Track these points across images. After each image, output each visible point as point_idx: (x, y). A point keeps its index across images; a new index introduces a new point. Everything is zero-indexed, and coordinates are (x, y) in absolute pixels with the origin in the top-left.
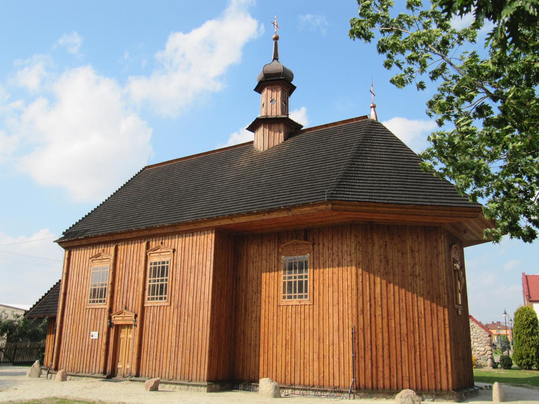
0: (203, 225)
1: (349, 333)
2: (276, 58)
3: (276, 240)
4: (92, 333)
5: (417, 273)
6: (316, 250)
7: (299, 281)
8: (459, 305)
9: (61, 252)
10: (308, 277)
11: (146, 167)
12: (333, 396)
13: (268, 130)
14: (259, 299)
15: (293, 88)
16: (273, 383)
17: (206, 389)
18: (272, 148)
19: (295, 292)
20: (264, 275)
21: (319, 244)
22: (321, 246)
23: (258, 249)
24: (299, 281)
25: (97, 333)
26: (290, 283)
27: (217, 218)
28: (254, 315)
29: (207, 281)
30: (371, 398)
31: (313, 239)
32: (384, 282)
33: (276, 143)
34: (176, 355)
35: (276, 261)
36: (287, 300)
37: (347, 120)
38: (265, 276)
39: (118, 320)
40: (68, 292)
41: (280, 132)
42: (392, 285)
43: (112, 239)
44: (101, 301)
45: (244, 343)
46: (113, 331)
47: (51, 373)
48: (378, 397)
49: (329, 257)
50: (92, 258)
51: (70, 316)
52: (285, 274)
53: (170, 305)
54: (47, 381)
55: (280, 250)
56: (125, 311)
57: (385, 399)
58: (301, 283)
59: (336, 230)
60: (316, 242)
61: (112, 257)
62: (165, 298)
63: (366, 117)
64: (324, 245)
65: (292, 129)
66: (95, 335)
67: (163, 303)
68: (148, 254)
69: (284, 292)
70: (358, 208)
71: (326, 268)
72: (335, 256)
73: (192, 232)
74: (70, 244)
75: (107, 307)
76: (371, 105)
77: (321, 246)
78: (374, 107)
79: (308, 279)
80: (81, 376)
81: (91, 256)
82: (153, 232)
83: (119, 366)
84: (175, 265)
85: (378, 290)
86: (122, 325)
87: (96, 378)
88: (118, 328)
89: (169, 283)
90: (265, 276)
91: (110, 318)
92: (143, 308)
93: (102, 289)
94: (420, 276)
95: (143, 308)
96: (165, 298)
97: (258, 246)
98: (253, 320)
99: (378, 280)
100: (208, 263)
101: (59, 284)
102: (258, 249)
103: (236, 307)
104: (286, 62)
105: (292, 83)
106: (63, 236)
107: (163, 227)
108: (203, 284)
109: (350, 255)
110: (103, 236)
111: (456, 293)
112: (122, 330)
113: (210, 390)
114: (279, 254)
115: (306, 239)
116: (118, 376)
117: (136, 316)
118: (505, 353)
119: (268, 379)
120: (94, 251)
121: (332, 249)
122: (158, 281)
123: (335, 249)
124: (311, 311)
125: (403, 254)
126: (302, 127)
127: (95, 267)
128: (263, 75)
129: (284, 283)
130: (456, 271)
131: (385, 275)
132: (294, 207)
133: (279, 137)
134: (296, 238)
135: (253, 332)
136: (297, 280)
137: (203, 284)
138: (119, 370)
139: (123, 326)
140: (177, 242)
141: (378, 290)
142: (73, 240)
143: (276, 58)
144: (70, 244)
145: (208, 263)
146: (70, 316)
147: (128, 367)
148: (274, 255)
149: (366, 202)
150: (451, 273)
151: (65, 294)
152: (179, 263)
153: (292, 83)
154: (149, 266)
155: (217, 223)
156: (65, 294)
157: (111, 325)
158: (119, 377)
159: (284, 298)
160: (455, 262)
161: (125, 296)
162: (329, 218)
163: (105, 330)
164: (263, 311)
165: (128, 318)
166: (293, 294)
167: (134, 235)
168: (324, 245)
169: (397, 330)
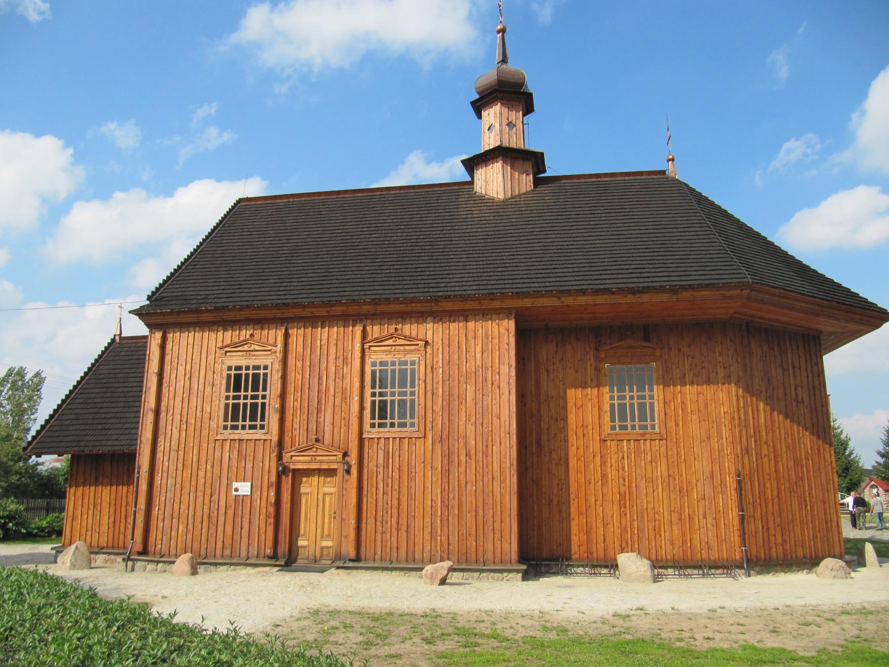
0: (496, 304)
1: (731, 482)
4: (235, 485)
7: (251, 404)
10: (268, 397)
12: (708, 574)
13: (509, 168)
14: (565, 428)
17: (520, 575)
18: (519, 195)
19: (244, 420)
20: (568, 391)
23: (556, 352)
24: (380, 401)
25: (249, 484)
26: (236, 407)
28: (554, 455)
29: (505, 397)
30: (769, 573)
32: (768, 408)
33: (523, 190)
34: (445, 521)
36: (377, 429)
37: (621, 173)
38: (573, 395)
40: (163, 408)
41: (527, 175)
42: (776, 413)
43: (279, 315)
45: (538, 499)
46: (287, 483)
47: (133, 560)
48: (776, 572)
50: (226, 347)
51: (173, 455)
52: (612, 391)
53: (425, 437)
54: (128, 574)
57: (783, 574)
58: (254, 406)
59: (701, 329)
61: (280, 346)
63: (664, 172)
68: (367, 346)
69: (373, 417)
70: (776, 299)
71: (685, 385)
73: (465, 315)
75: (275, 438)
76: (671, 157)
80: (216, 564)
81: (220, 345)
82: (382, 308)
83: (301, 543)
85: (762, 420)
86: (304, 470)
87: (255, 565)
88: (298, 475)
89: (419, 400)
90: (573, 395)
91: (280, 457)
97: (557, 346)
98: (554, 462)
99: (761, 404)
100: (505, 369)
102: (556, 352)
106: (148, 302)
110: (262, 307)
112: (304, 479)
113: (526, 576)
114: (599, 360)
115: (647, 339)
116: (299, 561)
119: (634, 554)
120: (229, 336)
128: (496, 82)
131: (769, 400)
132: (684, 288)
135: (555, 482)
136: (249, 401)
138: (301, 551)
139: (309, 473)
140: (430, 330)
141: (762, 420)
143: (504, 60)
145: (505, 369)
146: (173, 455)
148: (590, 361)
151: (157, 412)
154: (368, 369)
157: (283, 471)
158: (300, 562)
159: (373, 426)
163: (273, 479)
164: (572, 450)
167: (337, 310)
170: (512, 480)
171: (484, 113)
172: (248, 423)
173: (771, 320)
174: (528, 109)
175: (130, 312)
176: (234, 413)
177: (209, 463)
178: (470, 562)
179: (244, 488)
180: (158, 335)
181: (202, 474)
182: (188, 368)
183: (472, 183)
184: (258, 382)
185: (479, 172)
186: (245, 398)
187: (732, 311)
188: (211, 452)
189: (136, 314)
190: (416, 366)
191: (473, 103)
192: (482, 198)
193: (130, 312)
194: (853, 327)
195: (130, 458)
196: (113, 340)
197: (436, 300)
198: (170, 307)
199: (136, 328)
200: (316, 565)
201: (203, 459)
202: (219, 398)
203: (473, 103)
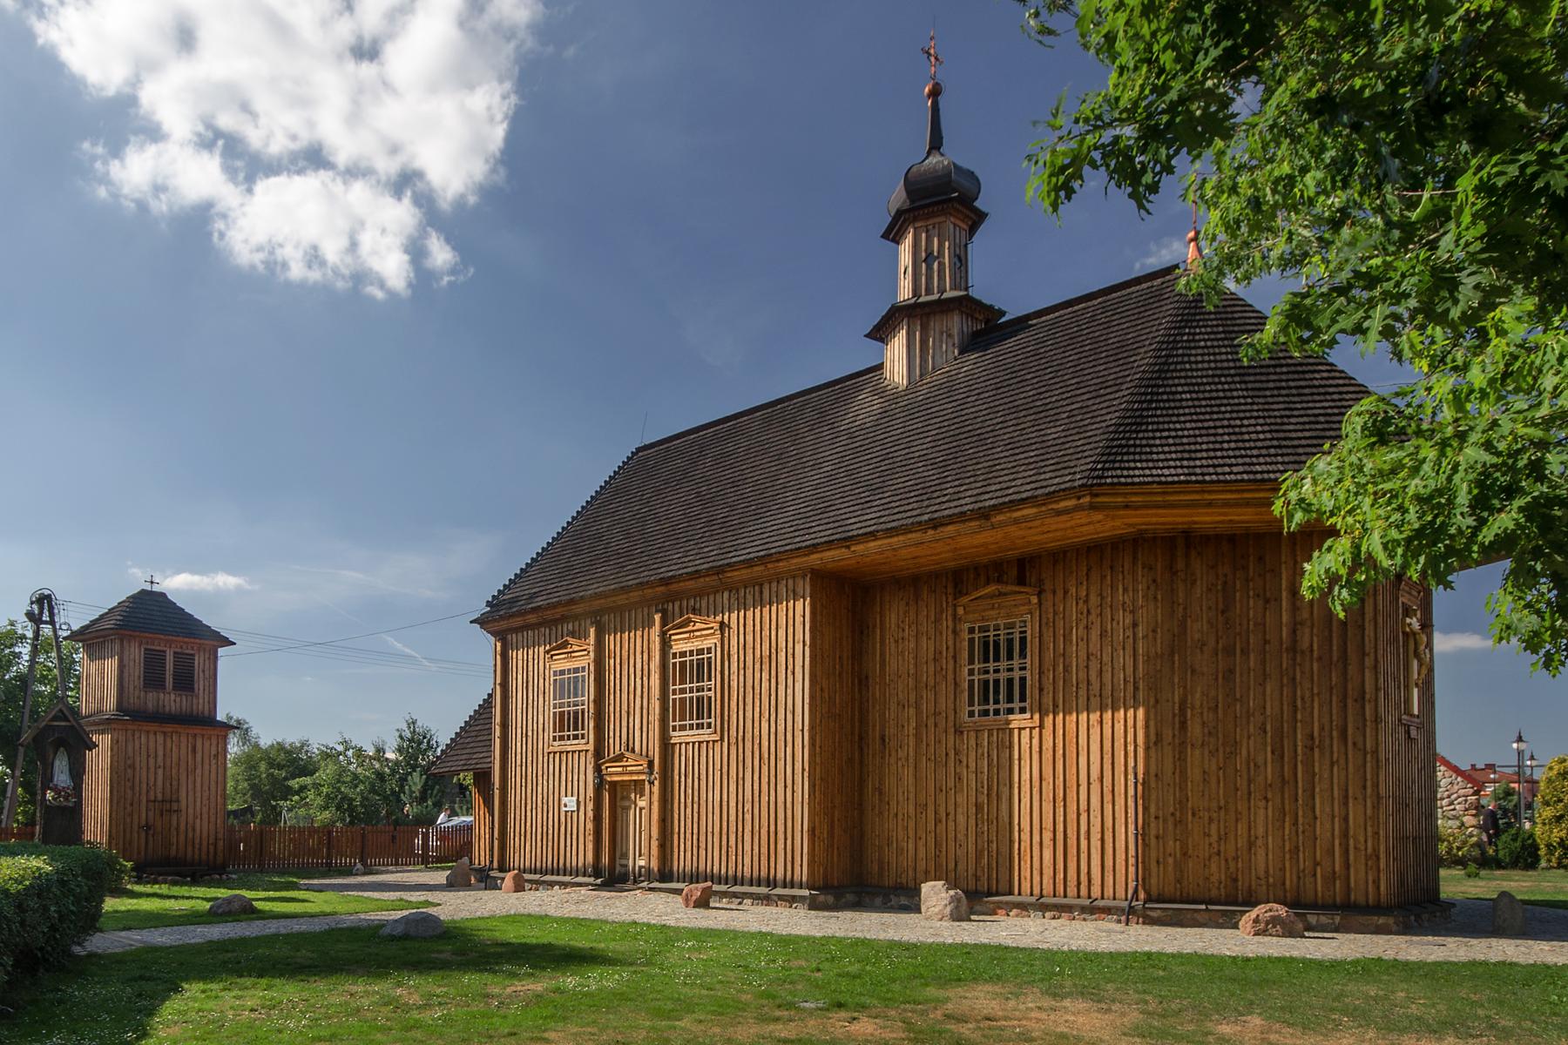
2: (936, 144)
3: (950, 590)
5: (1305, 645)
6: (1048, 605)
8: (1412, 715)
9: (485, 645)
11: (639, 450)
15: (981, 216)
16: (952, 892)
21: (1054, 592)
22: (1060, 594)
27: (814, 548)
31: (1041, 581)
35: (951, 637)
39: (614, 773)
44: (576, 737)
49: (1078, 621)
53: (722, 739)
55: (960, 611)
56: (627, 754)
60: (1048, 586)
62: (709, 726)
64: (1066, 592)
65: (987, 328)
66: (570, 802)
67: (705, 735)
72: (1092, 617)
74: (504, 625)
75: (591, 747)
77: (1060, 594)
78: (1035, 123)
79: (1028, 674)
84: (726, 656)
91: (598, 769)
92: (667, 747)
93: (576, 713)
94: (1312, 651)
95: (667, 747)
96: (709, 726)
101: (488, 703)
103: (861, 738)
104: (955, 153)
105: (977, 204)
107: (696, 575)
108: (790, 691)
109: (1132, 612)
111: (1407, 687)
115: (1021, 581)
117: (651, 764)
118: (1154, 26)
121: (1086, 602)
122: (689, 693)
123: (1094, 600)
124: (1036, 741)
125: (1267, 601)
126: (1003, 313)
127: (552, 670)
129: (971, 683)
130: (1409, 635)
133: (944, 353)
134: (999, 581)
137: (790, 691)
142: (515, 617)
143: (936, 144)
144: (504, 625)
147: (642, 863)
149: (1180, 482)
150: (1396, 639)
152: (734, 650)
153: (977, 204)
155: (814, 559)
156: (505, 725)
160: (1408, 612)
161: (624, 724)
162: (1084, 529)
165: (633, 768)
166: (992, 707)
168: (1066, 592)
169: (1246, 826)
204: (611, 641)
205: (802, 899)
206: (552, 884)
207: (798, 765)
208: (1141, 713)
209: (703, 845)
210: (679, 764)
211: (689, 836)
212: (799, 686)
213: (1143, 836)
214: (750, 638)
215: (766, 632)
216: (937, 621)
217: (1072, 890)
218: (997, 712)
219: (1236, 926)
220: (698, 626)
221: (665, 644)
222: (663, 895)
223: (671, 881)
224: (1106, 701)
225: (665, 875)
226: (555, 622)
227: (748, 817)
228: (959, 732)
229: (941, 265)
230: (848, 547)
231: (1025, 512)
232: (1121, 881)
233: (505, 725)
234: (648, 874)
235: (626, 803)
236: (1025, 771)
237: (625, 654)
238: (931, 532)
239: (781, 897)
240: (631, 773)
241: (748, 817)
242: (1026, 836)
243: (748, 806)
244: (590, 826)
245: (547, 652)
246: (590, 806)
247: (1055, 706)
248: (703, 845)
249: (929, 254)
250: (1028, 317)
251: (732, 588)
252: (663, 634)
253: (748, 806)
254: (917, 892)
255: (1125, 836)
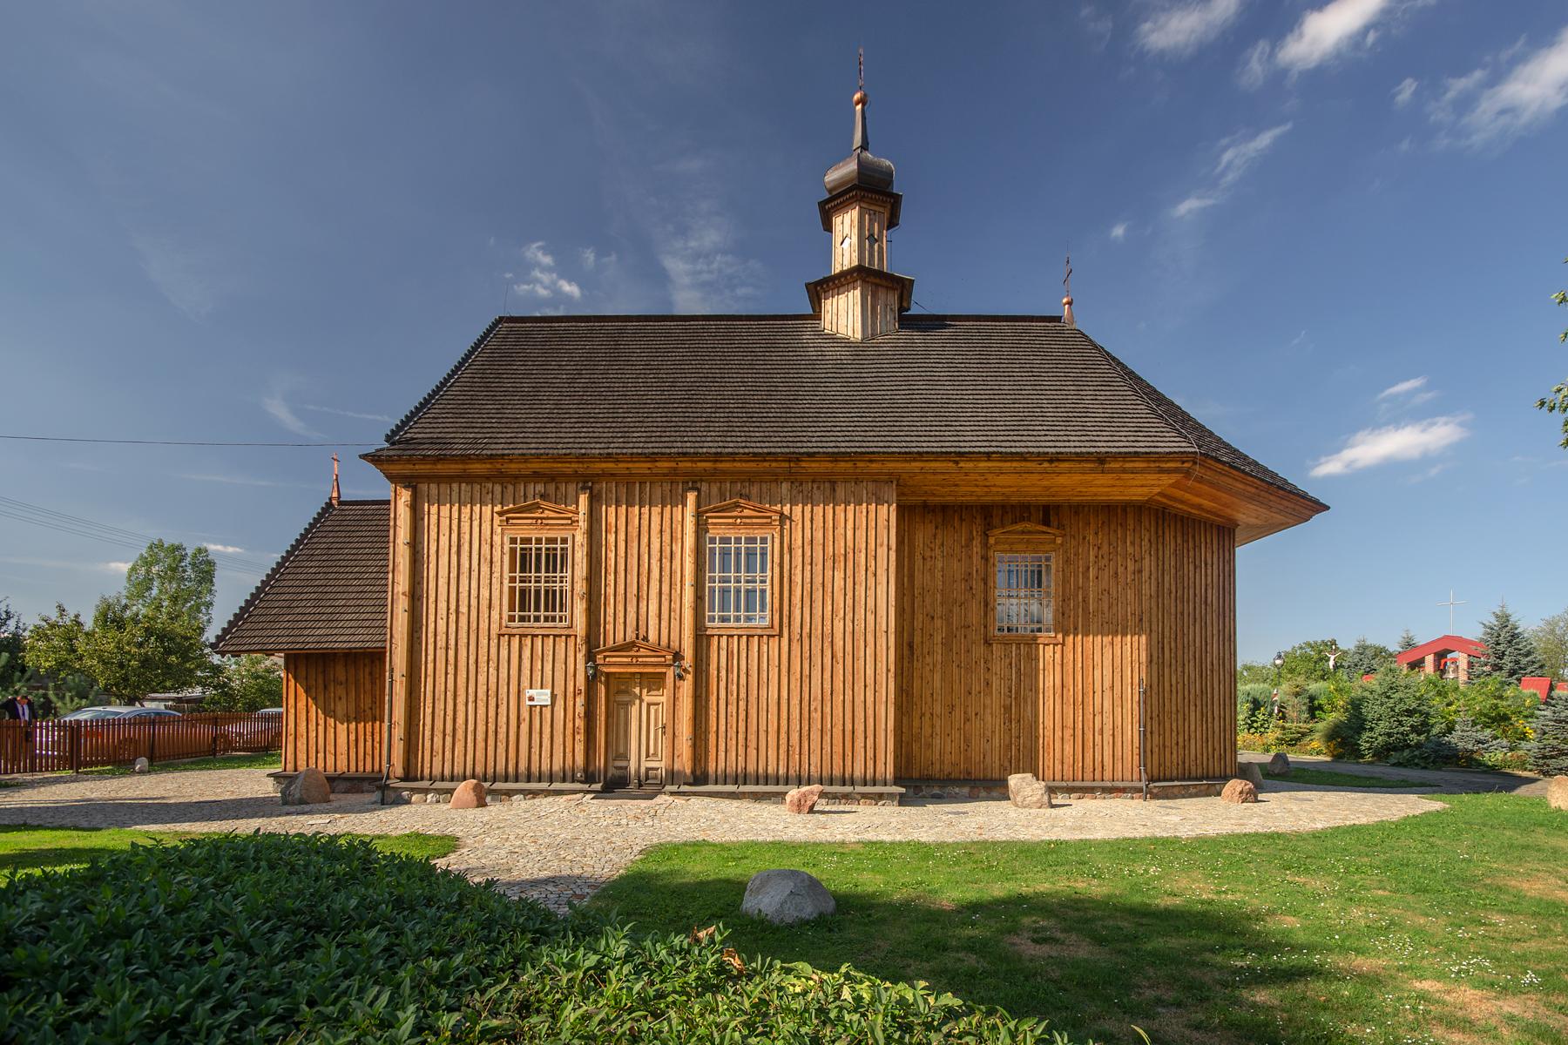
4: (529, 692)
11: (501, 319)
23: (935, 536)
25: (548, 691)
39: (615, 664)
53: (780, 635)
63: (1058, 319)
91: (590, 657)
92: (701, 638)
106: (387, 445)
113: (903, 801)
115: (1046, 523)
166: (732, 614)
170: (209, 797)
171: (837, 221)
172: (542, 613)
173: (1193, 506)
174: (892, 223)
175: (364, 457)
176: (522, 600)
177: (493, 665)
178: (843, 787)
179: (542, 696)
180: (405, 496)
181: (482, 679)
182: (454, 536)
183: (817, 316)
184: (555, 560)
185: (829, 302)
186: (538, 581)
187: (1157, 490)
188: (493, 650)
189: (372, 461)
190: (769, 545)
191: (822, 204)
192: (833, 338)
193: (364, 457)
194: (1279, 518)
195: (375, 658)
196: (329, 505)
197: (796, 458)
198: (423, 457)
199: (371, 485)
200: (648, 786)
201: (483, 659)
202: (498, 584)
203: (822, 204)
204: (609, 513)
205: (891, 796)
206: (509, 793)
207: (882, 667)
208: (1143, 638)
209: (752, 744)
210: (717, 657)
211: (732, 733)
212: (882, 589)
213: (1145, 735)
214: (819, 535)
215: (840, 530)
216: (969, 544)
217: (1089, 775)
218: (738, 619)
219: (1219, 794)
220: (746, 512)
221: (701, 529)
222: (707, 800)
223: (706, 783)
224: (1115, 627)
225: (699, 777)
226: (516, 478)
227: (816, 716)
228: (988, 643)
229: (881, 248)
230: (957, 463)
231: (1137, 465)
232: (1129, 765)
233: (415, 596)
234: (673, 776)
235: (626, 698)
236: (1049, 680)
237: (634, 532)
238: (1046, 465)
239: (865, 796)
240: (645, 665)
241: (816, 716)
242: (1049, 733)
243: (816, 704)
244: (580, 723)
245: (501, 514)
246: (580, 700)
247: (1076, 629)
248: (752, 744)
249: (872, 235)
250: (945, 318)
251: (795, 479)
252: (698, 515)
253: (816, 704)
254: (1003, 783)
255: (1131, 733)
